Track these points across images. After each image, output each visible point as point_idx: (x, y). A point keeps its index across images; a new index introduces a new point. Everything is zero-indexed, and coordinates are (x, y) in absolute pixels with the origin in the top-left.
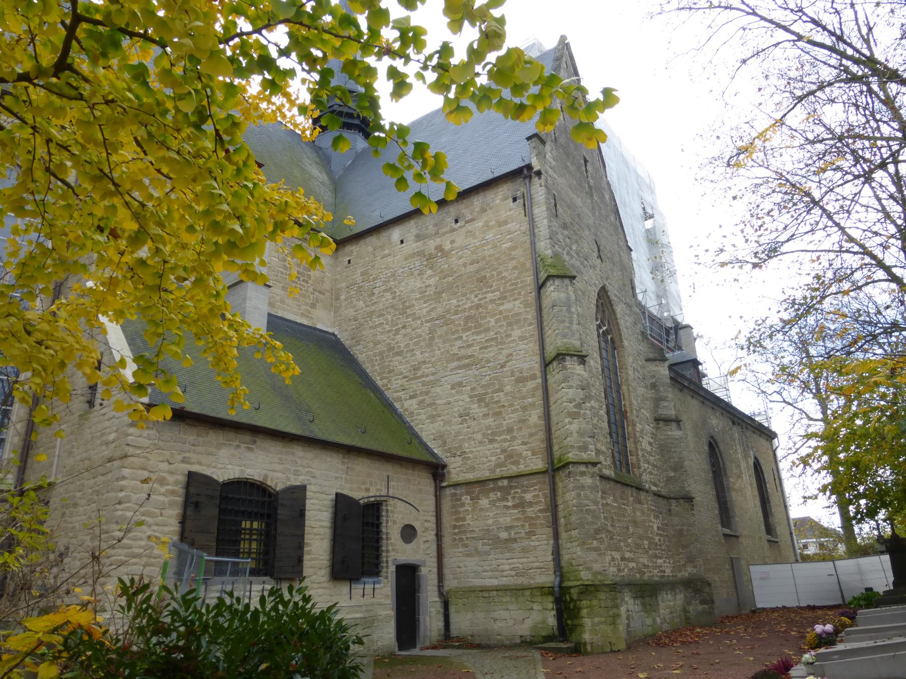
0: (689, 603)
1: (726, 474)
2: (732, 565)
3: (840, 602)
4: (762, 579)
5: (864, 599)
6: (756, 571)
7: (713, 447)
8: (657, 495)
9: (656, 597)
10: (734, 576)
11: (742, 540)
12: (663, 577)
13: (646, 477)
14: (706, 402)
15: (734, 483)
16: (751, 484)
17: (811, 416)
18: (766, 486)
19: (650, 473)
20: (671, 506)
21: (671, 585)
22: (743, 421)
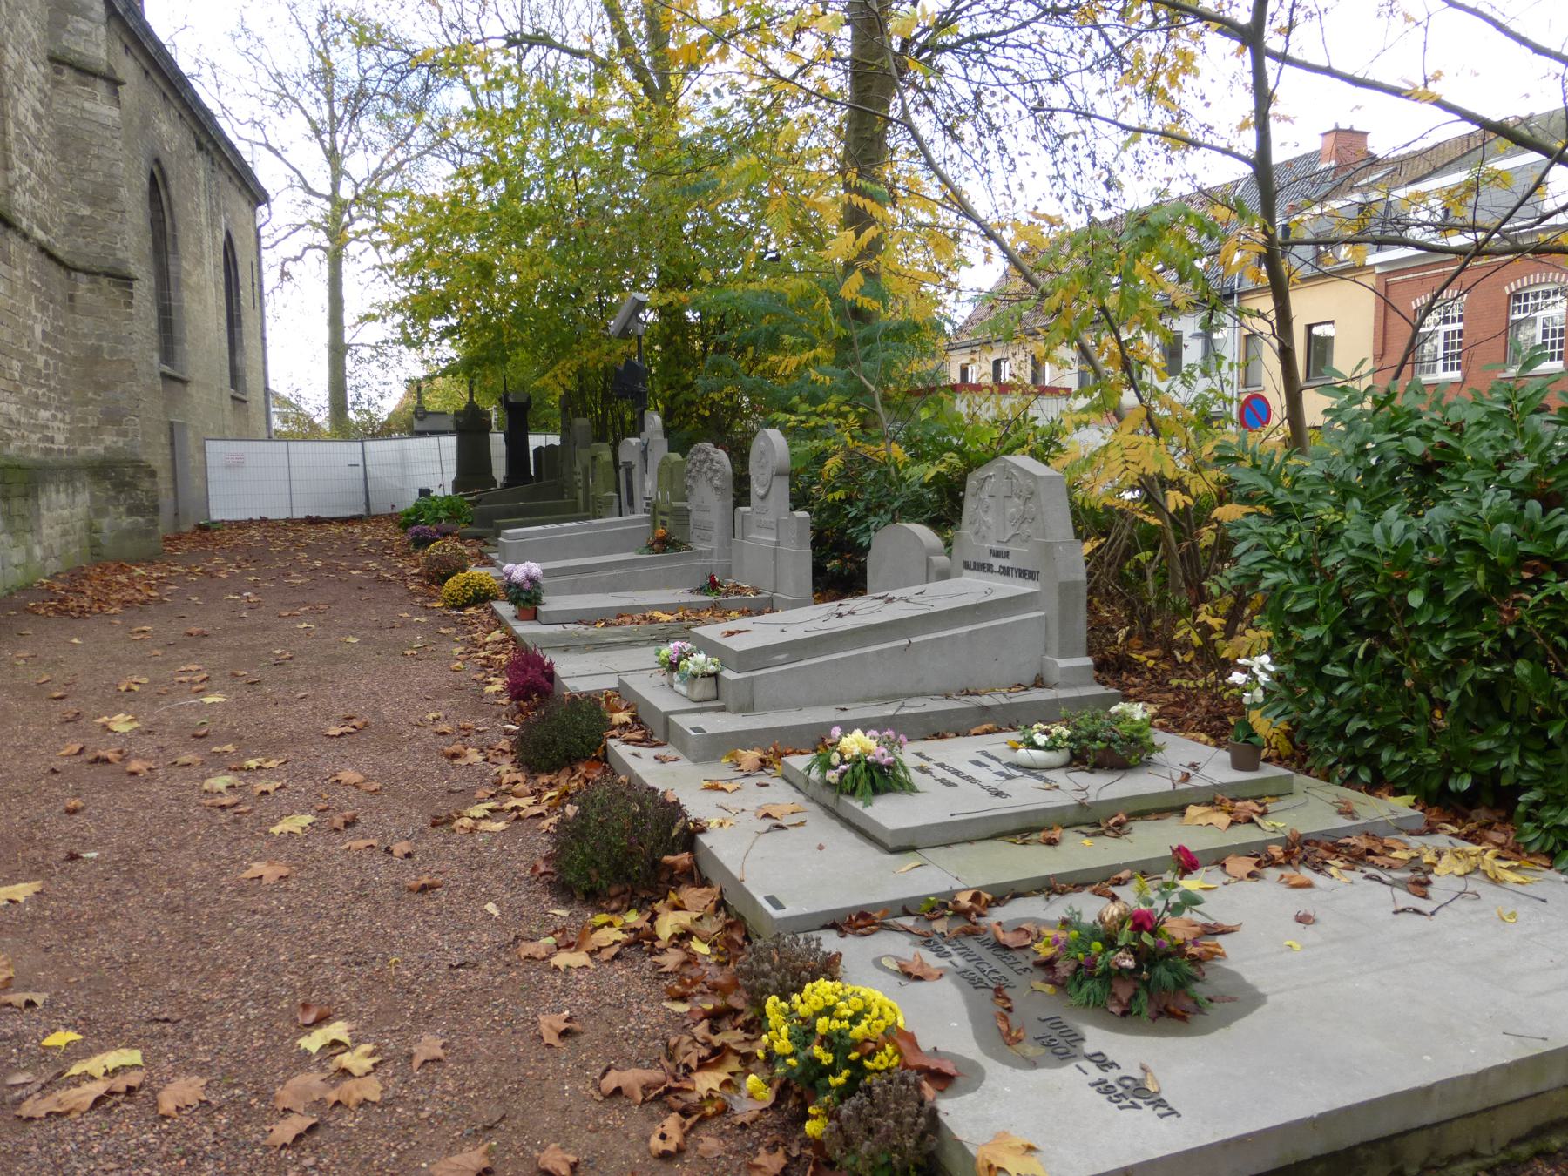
0: (100, 512)
1: (176, 251)
2: (172, 437)
3: (361, 511)
4: (228, 467)
5: (447, 509)
6: (217, 451)
7: (157, 185)
8: (44, 250)
9: (36, 498)
10: (173, 460)
11: (191, 389)
12: (48, 451)
13: (21, 199)
14: (152, 73)
15: (189, 274)
16: (216, 284)
17: (311, 185)
18: (238, 294)
19: (33, 192)
20: (75, 287)
21: (1411, 434)
22: (217, 148)
